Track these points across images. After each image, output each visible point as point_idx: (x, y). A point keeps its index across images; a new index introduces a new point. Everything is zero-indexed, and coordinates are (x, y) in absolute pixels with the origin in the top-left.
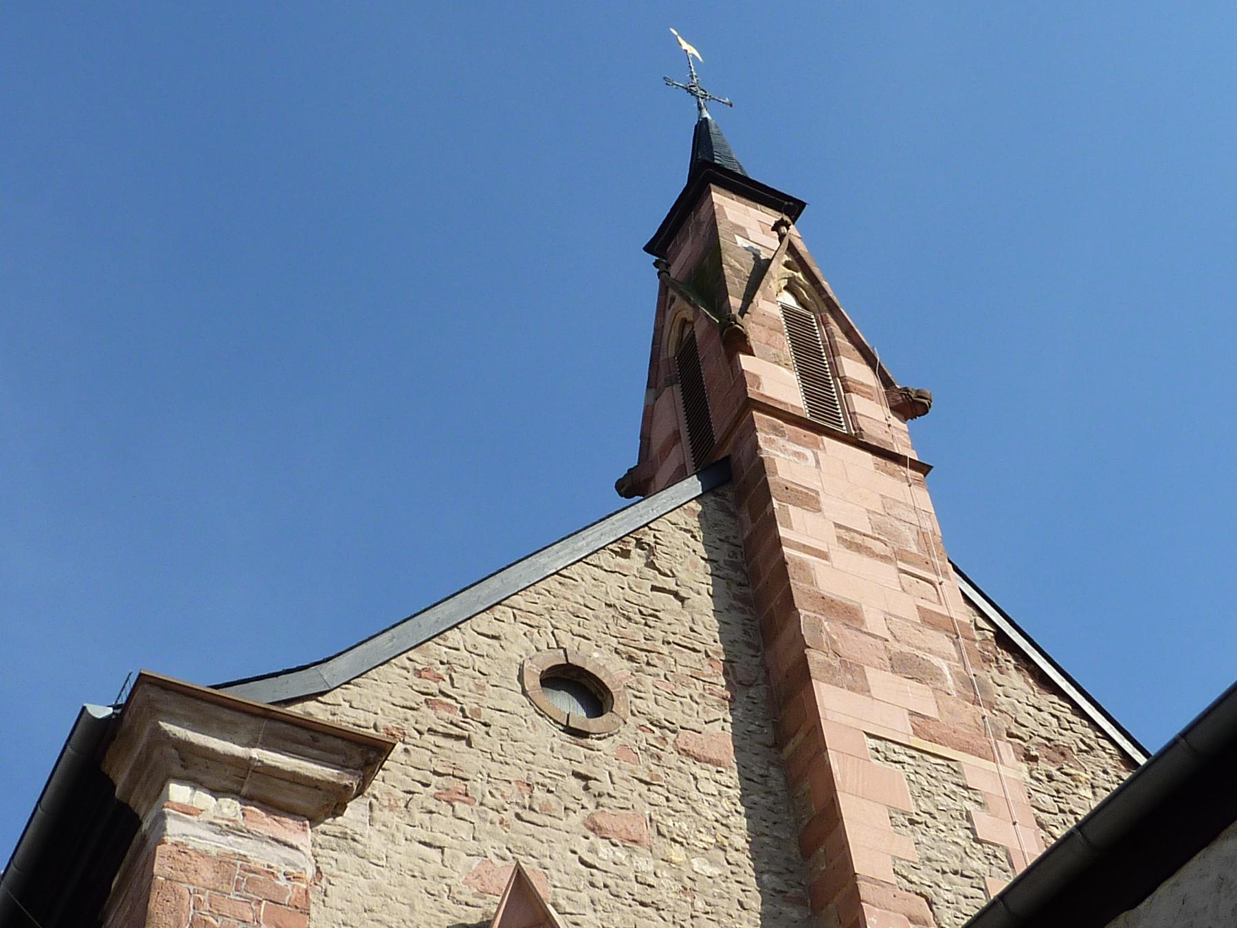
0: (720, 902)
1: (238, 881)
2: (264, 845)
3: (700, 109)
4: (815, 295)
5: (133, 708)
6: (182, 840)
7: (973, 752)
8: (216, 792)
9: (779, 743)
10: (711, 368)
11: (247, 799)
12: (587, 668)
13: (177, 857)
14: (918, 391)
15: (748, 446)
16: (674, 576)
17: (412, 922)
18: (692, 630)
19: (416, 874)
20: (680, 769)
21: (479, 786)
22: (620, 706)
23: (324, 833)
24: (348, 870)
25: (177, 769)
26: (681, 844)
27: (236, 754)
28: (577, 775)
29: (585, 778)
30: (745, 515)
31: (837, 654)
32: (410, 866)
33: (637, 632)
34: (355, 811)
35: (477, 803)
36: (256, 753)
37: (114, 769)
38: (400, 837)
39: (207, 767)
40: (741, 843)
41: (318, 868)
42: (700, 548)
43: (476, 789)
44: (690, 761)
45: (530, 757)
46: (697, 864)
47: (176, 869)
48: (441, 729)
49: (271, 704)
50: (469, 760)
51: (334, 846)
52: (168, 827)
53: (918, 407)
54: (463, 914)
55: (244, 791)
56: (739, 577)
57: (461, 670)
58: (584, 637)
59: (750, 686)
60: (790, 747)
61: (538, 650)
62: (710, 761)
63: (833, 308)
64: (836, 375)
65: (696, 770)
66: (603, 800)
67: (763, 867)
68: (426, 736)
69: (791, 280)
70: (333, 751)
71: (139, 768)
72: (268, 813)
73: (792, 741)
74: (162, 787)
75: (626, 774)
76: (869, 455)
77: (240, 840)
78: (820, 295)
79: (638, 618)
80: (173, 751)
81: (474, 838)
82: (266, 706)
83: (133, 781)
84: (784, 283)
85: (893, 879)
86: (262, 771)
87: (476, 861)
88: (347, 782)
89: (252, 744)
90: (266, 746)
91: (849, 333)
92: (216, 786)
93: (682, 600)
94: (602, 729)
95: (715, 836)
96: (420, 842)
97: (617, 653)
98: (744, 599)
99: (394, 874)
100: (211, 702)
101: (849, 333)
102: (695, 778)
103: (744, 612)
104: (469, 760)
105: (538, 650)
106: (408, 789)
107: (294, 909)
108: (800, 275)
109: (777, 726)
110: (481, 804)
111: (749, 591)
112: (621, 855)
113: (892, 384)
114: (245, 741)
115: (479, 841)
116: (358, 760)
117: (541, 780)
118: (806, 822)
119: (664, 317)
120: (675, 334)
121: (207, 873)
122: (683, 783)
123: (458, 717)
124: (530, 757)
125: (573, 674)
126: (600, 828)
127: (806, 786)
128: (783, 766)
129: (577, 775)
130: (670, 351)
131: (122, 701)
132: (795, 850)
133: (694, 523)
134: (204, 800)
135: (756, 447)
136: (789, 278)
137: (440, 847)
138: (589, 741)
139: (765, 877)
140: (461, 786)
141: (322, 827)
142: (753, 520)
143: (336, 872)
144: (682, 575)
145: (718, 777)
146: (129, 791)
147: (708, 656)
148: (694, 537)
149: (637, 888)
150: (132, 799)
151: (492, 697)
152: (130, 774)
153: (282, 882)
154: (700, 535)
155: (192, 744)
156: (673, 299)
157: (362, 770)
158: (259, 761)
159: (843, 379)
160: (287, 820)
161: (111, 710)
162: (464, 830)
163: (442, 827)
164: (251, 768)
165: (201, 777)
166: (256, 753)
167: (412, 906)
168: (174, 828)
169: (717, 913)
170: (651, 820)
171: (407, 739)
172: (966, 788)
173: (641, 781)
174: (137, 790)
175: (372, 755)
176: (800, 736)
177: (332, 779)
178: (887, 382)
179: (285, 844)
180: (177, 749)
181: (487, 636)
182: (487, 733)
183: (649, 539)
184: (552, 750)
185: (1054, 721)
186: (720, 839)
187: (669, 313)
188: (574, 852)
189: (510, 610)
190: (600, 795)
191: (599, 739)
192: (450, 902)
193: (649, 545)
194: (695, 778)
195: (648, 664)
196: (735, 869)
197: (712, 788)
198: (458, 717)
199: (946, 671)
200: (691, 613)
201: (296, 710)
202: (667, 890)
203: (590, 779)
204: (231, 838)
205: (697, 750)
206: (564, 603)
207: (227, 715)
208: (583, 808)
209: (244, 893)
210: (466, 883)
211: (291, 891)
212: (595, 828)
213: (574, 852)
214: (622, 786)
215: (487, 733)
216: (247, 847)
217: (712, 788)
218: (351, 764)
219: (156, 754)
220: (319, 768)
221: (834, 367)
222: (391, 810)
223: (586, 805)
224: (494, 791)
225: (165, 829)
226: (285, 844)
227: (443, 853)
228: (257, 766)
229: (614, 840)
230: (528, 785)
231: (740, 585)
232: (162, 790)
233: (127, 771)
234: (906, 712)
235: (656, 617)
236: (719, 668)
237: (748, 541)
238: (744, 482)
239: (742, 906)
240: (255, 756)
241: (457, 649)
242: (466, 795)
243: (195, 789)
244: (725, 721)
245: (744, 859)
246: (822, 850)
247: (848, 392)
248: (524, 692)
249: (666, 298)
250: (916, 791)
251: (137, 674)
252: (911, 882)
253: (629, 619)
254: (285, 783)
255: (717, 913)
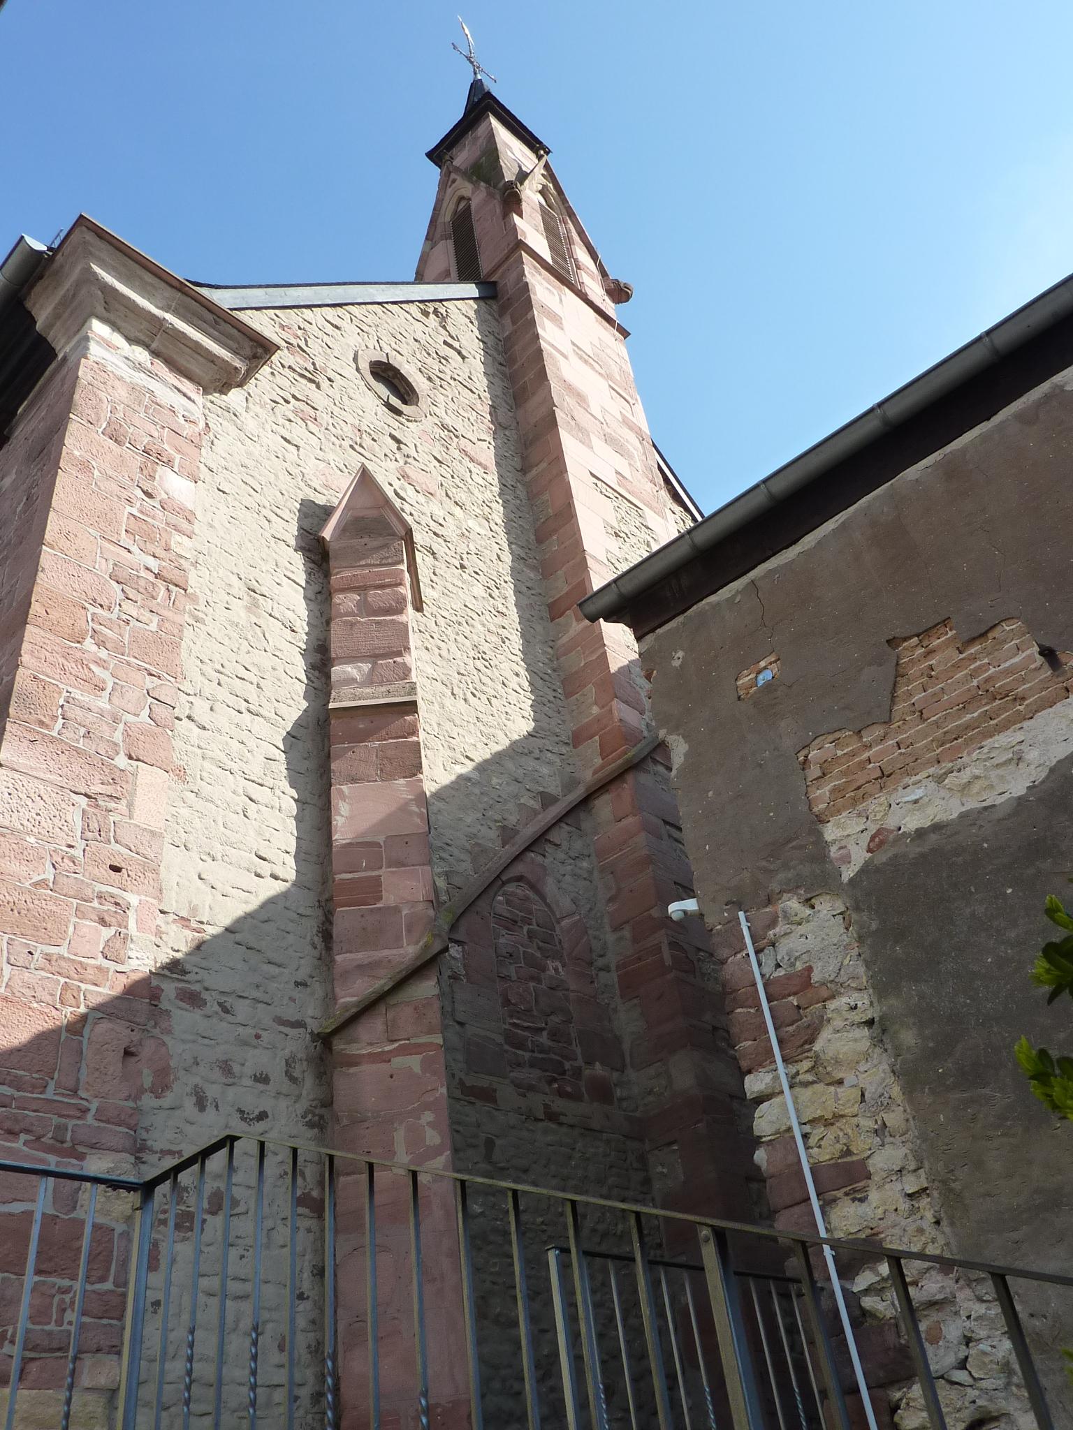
0: (485, 550)
1: (146, 406)
2: (168, 390)
3: (475, 74)
4: (560, 203)
5: (67, 249)
6: (103, 361)
7: (651, 508)
8: (131, 340)
9: (524, 471)
10: (484, 227)
11: (155, 354)
12: (402, 371)
13: (98, 372)
14: (625, 284)
15: (513, 276)
16: (458, 341)
17: (276, 486)
18: (469, 378)
19: (279, 456)
20: (460, 461)
21: (325, 418)
22: (424, 403)
23: (212, 402)
24: (230, 434)
25: (100, 309)
26: (461, 507)
27: (152, 311)
28: (393, 437)
29: (398, 441)
30: (507, 320)
31: (573, 418)
32: (276, 449)
33: (433, 364)
34: (235, 397)
35: (323, 428)
36: (168, 316)
37: (37, 306)
38: (268, 427)
39: (126, 316)
40: (499, 522)
41: (207, 424)
42: (477, 333)
43: (323, 418)
44: (467, 459)
45: (361, 413)
46: (472, 523)
47: (97, 380)
48: (298, 370)
49: (187, 280)
50: (317, 397)
51: (220, 414)
52: (91, 348)
53: (623, 294)
54: (312, 495)
55: (154, 346)
56: (500, 359)
57: (313, 337)
58: (399, 352)
59: (506, 428)
60: (534, 472)
61: (367, 347)
62: (480, 464)
63: (572, 215)
64: (571, 256)
65: (471, 465)
66: (409, 460)
67: (512, 540)
68: (286, 369)
69: (544, 187)
70: (230, 337)
71: (64, 303)
72: (171, 370)
73: (535, 469)
74: (84, 322)
75: (426, 450)
76: (591, 311)
77: (149, 378)
78: (563, 204)
79: (435, 356)
80: (99, 293)
81: (321, 449)
82: (183, 281)
83: (56, 316)
84: (540, 187)
85: (606, 562)
86: (170, 333)
87: (322, 465)
88: (238, 366)
89: (167, 309)
90: (176, 313)
91: (581, 233)
92: (132, 335)
93: (463, 358)
94: (411, 414)
95: (483, 510)
96: (282, 437)
97: (421, 372)
98: (504, 374)
99: (264, 450)
100: (137, 262)
101: (581, 233)
102: (470, 471)
103: (503, 381)
104: (317, 397)
105: (367, 347)
106: (274, 399)
107: (190, 442)
108: (551, 185)
109: (524, 458)
110: (326, 429)
111: (507, 370)
112: (421, 498)
113: (607, 275)
114: (160, 305)
115: (324, 452)
116: (248, 352)
117: (368, 430)
118: (542, 520)
119: (445, 193)
120: (452, 207)
121: (122, 393)
122: (462, 470)
123: (311, 368)
124: (361, 413)
125: (390, 374)
126: (408, 477)
127: (546, 497)
128: (527, 485)
129: (393, 437)
130: (447, 216)
131: (55, 245)
132: (533, 537)
133: (472, 314)
134: (118, 340)
135: (523, 274)
136: (543, 185)
137: (296, 446)
138: (401, 418)
139: (513, 546)
140: (312, 412)
141: (210, 397)
142: (514, 323)
143: (221, 432)
144: (463, 342)
145: (485, 476)
146: (50, 326)
147: (480, 398)
148: (472, 322)
149: (432, 523)
150: (51, 333)
151: (333, 364)
152: (55, 308)
153: (181, 420)
154: (476, 323)
155: (117, 290)
156: (454, 181)
157: (249, 360)
158: (171, 324)
159: (576, 260)
160: (185, 381)
161: (45, 248)
162: (313, 441)
163: (297, 432)
164: (163, 328)
165: (119, 322)
166: (168, 316)
167: (276, 475)
168: (95, 350)
169: (484, 556)
170: (442, 485)
171: (273, 366)
172: (648, 528)
173: (436, 458)
174: (58, 324)
175: (260, 350)
176: (543, 465)
177: (226, 358)
178: (604, 274)
179: (185, 395)
180: (103, 293)
181: (332, 324)
182: (331, 386)
183: (442, 310)
184: (376, 414)
185: (682, 522)
186: (486, 513)
187: (449, 191)
188: (391, 485)
189: (348, 315)
190: (408, 456)
191: (408, 420)
192: (303, 484)
193: (442, 315)
194: (470, 471)
195: (441, 386)
196: (496, 535)
197: (481, 482)
198: (311, 368)
199: (636, 456)
200: (469, 368)
201: (204, 291)
202: (450, 531)
203: (402, 443)
204: (142, 375)
205: (472, 454)
206: (386, 325)
207: (148, 277)
208: (396, 460)
209: (152, 417)
210: (314, 475)
211: (188, 430)
212: (405, 476)
213: (391, 485)
214: (423, 457)
215: (331, 386)
216: (153, 385)
217: (481, 482)
218: (242, 353)
219: (83, 292)
220: (217, 347)
221: (570, 250)
222: (261, 408)
223: (398, 459)
224: (336, 424)
225: (88, 349)
226: (185, 395)
227: (298, 450)
228: (168, 328)
229: (417, 488)
230: (359, 430)
231: (500, 364)
232: (83, 325)
233: (53, 305)
234: (614, 471)
235: (447, 360)
236: (487, 409)
237: (508, 338)
238: (508, 299)
239: (499, 558)
240: (167, 318)
241: (311, 324)
242: (316, 420)
243: (113, 331)
244: (489, 443)
245: (500, 530)
246: (555, 537)
247: (580, 269)
248: (358, 370)
249: (448, 180)
250: (620, 517)
251: (78, 215)
252: (617, 569)
253: (429, 354)
254: (188, 349)
255: (484, 556)
